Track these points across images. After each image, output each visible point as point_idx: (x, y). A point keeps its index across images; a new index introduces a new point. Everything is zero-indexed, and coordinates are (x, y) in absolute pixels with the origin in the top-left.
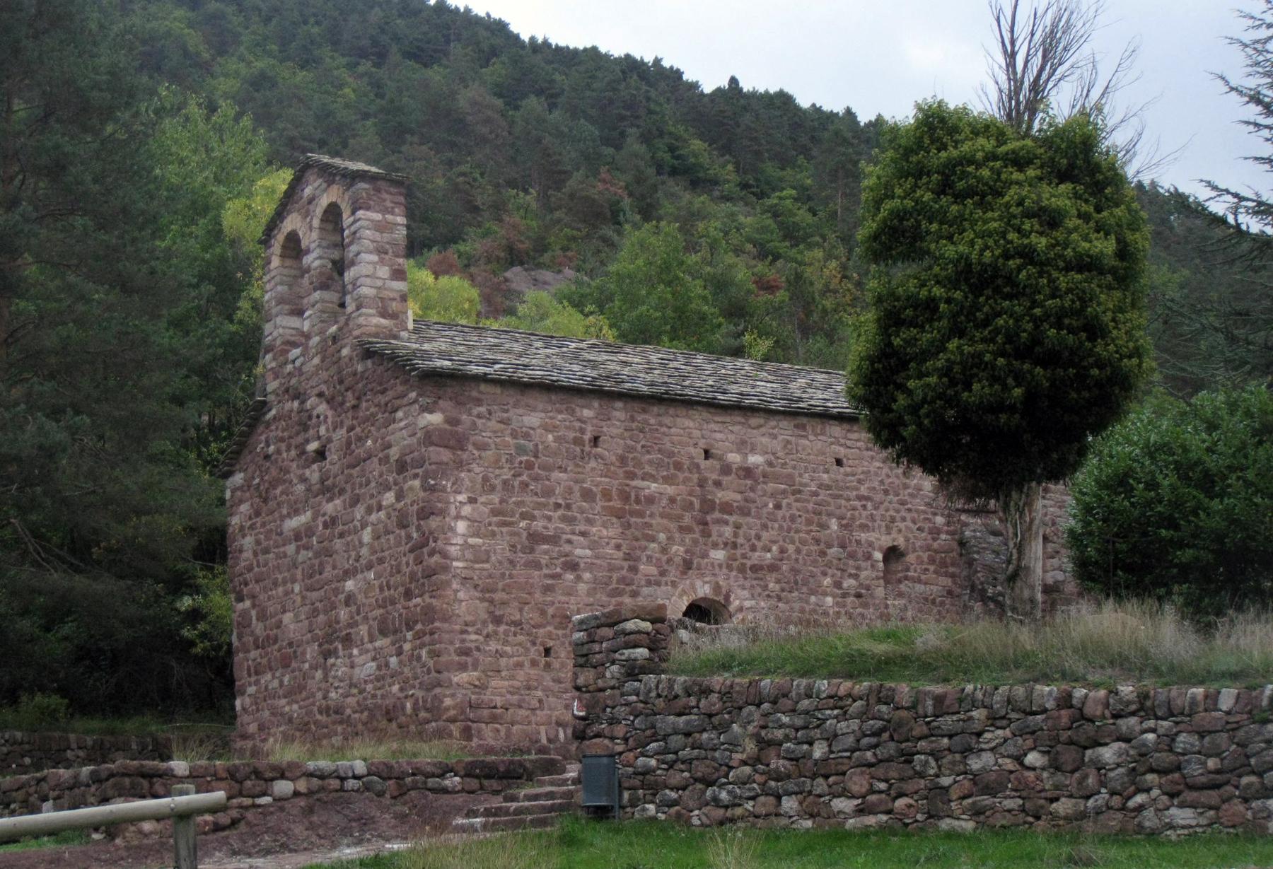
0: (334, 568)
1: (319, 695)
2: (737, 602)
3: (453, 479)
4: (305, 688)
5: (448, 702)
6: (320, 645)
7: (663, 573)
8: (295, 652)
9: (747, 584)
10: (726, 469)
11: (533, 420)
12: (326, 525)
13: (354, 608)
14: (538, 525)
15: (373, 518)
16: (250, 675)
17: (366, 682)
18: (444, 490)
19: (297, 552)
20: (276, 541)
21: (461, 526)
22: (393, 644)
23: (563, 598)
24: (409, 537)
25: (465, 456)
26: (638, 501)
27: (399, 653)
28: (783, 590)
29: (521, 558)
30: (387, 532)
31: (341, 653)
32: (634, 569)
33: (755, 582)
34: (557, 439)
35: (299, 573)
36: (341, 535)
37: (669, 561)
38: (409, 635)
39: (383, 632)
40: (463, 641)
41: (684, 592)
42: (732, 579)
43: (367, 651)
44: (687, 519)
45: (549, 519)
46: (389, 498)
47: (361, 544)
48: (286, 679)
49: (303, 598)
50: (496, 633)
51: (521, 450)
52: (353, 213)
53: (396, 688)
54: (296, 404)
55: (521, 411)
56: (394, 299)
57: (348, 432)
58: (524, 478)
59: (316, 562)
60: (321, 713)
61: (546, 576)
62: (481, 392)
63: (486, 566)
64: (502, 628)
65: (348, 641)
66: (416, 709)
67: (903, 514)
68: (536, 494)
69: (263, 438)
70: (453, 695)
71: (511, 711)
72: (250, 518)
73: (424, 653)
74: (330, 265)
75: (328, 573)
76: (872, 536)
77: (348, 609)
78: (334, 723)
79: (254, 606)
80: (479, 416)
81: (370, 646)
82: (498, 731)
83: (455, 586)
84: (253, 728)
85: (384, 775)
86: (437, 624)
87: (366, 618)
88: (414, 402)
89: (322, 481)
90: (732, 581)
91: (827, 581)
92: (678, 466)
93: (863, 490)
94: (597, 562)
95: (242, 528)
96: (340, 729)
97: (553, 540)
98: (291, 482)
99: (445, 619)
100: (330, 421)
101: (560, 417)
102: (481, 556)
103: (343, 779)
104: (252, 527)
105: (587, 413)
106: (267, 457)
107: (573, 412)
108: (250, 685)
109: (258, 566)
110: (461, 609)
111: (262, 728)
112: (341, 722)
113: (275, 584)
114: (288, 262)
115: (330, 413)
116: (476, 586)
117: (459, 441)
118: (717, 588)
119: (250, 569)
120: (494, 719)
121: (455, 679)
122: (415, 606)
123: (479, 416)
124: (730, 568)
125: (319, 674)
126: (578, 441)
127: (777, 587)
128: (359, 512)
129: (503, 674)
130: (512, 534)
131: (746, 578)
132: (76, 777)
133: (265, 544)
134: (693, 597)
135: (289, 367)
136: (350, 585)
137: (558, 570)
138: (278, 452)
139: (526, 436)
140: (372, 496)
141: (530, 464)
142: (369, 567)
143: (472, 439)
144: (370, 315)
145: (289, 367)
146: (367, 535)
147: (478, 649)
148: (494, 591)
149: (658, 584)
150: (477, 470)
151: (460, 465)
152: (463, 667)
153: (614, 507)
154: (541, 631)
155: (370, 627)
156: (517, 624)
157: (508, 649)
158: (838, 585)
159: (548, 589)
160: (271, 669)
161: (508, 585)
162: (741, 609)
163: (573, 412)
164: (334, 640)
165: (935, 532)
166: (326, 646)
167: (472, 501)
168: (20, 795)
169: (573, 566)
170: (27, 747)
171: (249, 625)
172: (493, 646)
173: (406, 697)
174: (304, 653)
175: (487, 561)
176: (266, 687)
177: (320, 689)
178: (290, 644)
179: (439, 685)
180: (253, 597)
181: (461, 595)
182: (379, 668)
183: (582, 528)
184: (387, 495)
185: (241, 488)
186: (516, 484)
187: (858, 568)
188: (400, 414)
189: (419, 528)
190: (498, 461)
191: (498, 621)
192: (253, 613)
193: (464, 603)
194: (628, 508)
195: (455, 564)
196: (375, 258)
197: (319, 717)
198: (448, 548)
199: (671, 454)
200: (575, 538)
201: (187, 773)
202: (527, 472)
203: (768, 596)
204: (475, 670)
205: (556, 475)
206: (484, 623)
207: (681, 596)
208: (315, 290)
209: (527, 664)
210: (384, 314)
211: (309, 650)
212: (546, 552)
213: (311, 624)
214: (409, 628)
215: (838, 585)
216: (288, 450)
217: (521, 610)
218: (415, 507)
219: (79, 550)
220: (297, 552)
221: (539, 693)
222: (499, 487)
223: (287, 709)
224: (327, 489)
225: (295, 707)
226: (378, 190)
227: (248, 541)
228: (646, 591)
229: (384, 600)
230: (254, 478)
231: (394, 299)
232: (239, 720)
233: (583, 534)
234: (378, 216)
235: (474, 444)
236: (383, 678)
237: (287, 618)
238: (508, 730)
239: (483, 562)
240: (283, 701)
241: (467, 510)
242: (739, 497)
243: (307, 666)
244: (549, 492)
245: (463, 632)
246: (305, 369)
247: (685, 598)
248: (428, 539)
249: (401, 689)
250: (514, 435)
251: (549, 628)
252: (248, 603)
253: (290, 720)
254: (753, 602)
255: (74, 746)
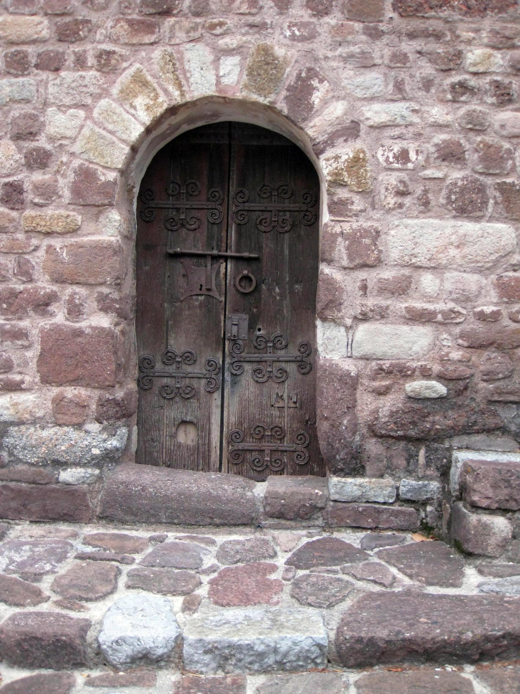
2: (337, 109)
7: (68, 33)
9: (381, 51)
33: (408, 47)
42: (324, 36)
90: (321, 47)
118: (264, 67)
127: (499, 60)
131: (375, 34)
134: (170, 96)
149: (52, 64)
162: (351, 130)
203: (462, 88)
207: (126, 96)
219: (368, 502)
247: (141, 101)
254: (400, 108)
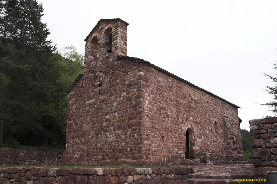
0: (102, 112)
1: (94, 144)
3: (145, 89)
4: (89, 142)
5: (143, 149)
6: (95, 132)
8: (86, 133)
10: (192, 100)
11: (161, 79)
12: (100, 102)
13: (108, 123)
14: (162, 105)
15: (118, 99)
16: (71, 138)
17: (111, 142)
18: (144, 91)
19: (90, 109)
20: (82, 107)
21: (147, 102)
22: (123, 132)
23: (166, 124)
24: (131, 104)
25: (148, 84)
26: (179, 103)
27: (126, 134)
28: (201, 128)
29: (159, 112)
30: (123, 102)
31: (103, 134)
32: (178, 119)
34: (165, 85)
35: (90, 114)
36: (105, 104)
37: (184, 118)
38: (130, 130)
39: (119, 129)
40: (147, 132)
41: (186, 126)
43: (112, 134)
44: (186, 110)
45: (164, 104)
46: (125, 94)
47: (112, 106)
48: (83, 140)
49: (91, 120)
50: (153, 131)
51: (159, 86)
52: (116, 28)
53: (123, 144)
54: (92, 74)
55: (159, 76)
56: (124, 49)
57: (110, 79)
58: (159, 92)
59: (96, 111)
60: (94, 149)
61: (163, 118)
62: (151, 70)
63: (152, 113)
64: (154, 130)
65: (105, 131)
66: (131, 150)
67: (216, 115)
68: (161, 97)
69: (81, 83)
70: (144, 147)
71: (156, 152)
72: (75, 101)
73: (136, 135)
74: (105, 43)
75: (100, 113)
76: (213, 119)
77: (106, 123)
78: (99, 152)
79: (74, 122)
80: (151, 75)
81: (114, 132)
82: (153, 157)
83: (145, 117)
84: (70, 151)
85: (156, 174)
86: (141, 127)
87: (113, 125)
88: (135, 69)
89: (100, 91)
91: (207, 127)
92: (185, 97)
93: (211, 109)
94: (172, 116)
95: (72, 104)
96: (101, 154)
97: (164, 109)
98: (89, 92)
99: (143, 126)
100: (104, 77)
101: (165, 80)
102: (151, 111)
103: (146, 175)
104: (75, 104)
105: (170, 80)
106: (82, 87)
107: (168, 80)
108: (71, 141)
109: (76, 112)
110: (147, 123)
111: (73, 151)
112: (102, 152)
113: (81, 117)
114: (92, 44)
115: (104, 75)
116: (149, 118)
117: (147, 80)
118: (191, 126)
119: (74, 113)
120: (153, 154)
121: (145, 142)
122: (133, 122)
123: (151, 75)
124: (193, 121)
125: (94, 139)
126: (169, 87)
128: (112, 98)
129: (155, 142)
130: (157, 106)
132: (47, 171)
133: (79, 107)
135: (91, 66)
136: (108, 117)
137: (165, 117)
138: (86, 86)
139: (159, 83)
140: (118, 94)
141: (160, 89)
142: (115, 112)
143: (149, 80)
144: (119, 51)
145: (91, 66)
146: (115, 104)
147: (150, 135)
148: (153, 120)
150: (150, 88)
151: (147, 86)
152: (147, 139)
153: (174, 103)
154: (162, 132)
155: (114, 128)
156: (157, 129)
157: (155, 135)
158: (209, 128)
159: (163, 121)
160: (78, 137)
161: (156, 119)
162: (195, 131)
163: (168, 80)
164: (100, 130)
165: (220, 120)
166: (98, 132)
167: (149, 96)
168: (17, 176)
169: (167, 116)
170: (10, 152)
171: (72, 126)
172: (152, 134)
173: (127, 147)
174: (90, 134)
175: (152, 112)
176: (76, 142)
177: (94, 143)
178: (85, 131)
179: (142, 144)
180: (74, 120)
181: (147, 120)
182: (117, 138)
183: (169, 107)
184: (124, 93)
185: (73, 95)
186: (158, 94)
187: (211, 125)
188: (130, 73)
189: (135, 101)
190: (154, 87)
191: (153, 127)
192: (74, 124)
193: (147, 122)
194: (177, 105)
195: (146, 111)
196: (121, 39)
197: (93, 150)
198: (144, 107)
199: (184, 94)
200: (168, 109)
201: (102, 173)
202: (160, 91)
204: (149, 140)
205: (165, 93)
206: (151, 128)
208: (101, 48)
209: (159, 140)
210: (122, 52)
211: (91, 133)
212: (163, 112)
213: (93, 126)
214: (130, 127)
215: (209, 128)
216: (89, 85)
217: (158, 126)
218: (135, 96)
220: (90, 109)
221: (161, 148)
222: (154, 94)
223: (82, 147)
224: (100, 93)
225: (85, 147)
226: (122, 25)
227: (74, 106)
228: (180, 125)
229: (120, 120)
230: (77, 92)
231: (124, 49)
232: (66, 149)
233: (170, 109)
234: (122, 30)
235: (150, 82)
236: (118, 141)
237: (84, 125)
238: (155, 157)
239: (151, 112)
240: (81, 145)
241: (148, 98)
242: (194, 106)
243: (90, 137)
244: (163, 97)
245: (147, 130)
246: (96, 66)
248: (139, 104)
249: (126, 144)
250: (157, 81)
251: (163, 131)
252: (72, 121)
253: (83, 150)
255: (21, 152)
